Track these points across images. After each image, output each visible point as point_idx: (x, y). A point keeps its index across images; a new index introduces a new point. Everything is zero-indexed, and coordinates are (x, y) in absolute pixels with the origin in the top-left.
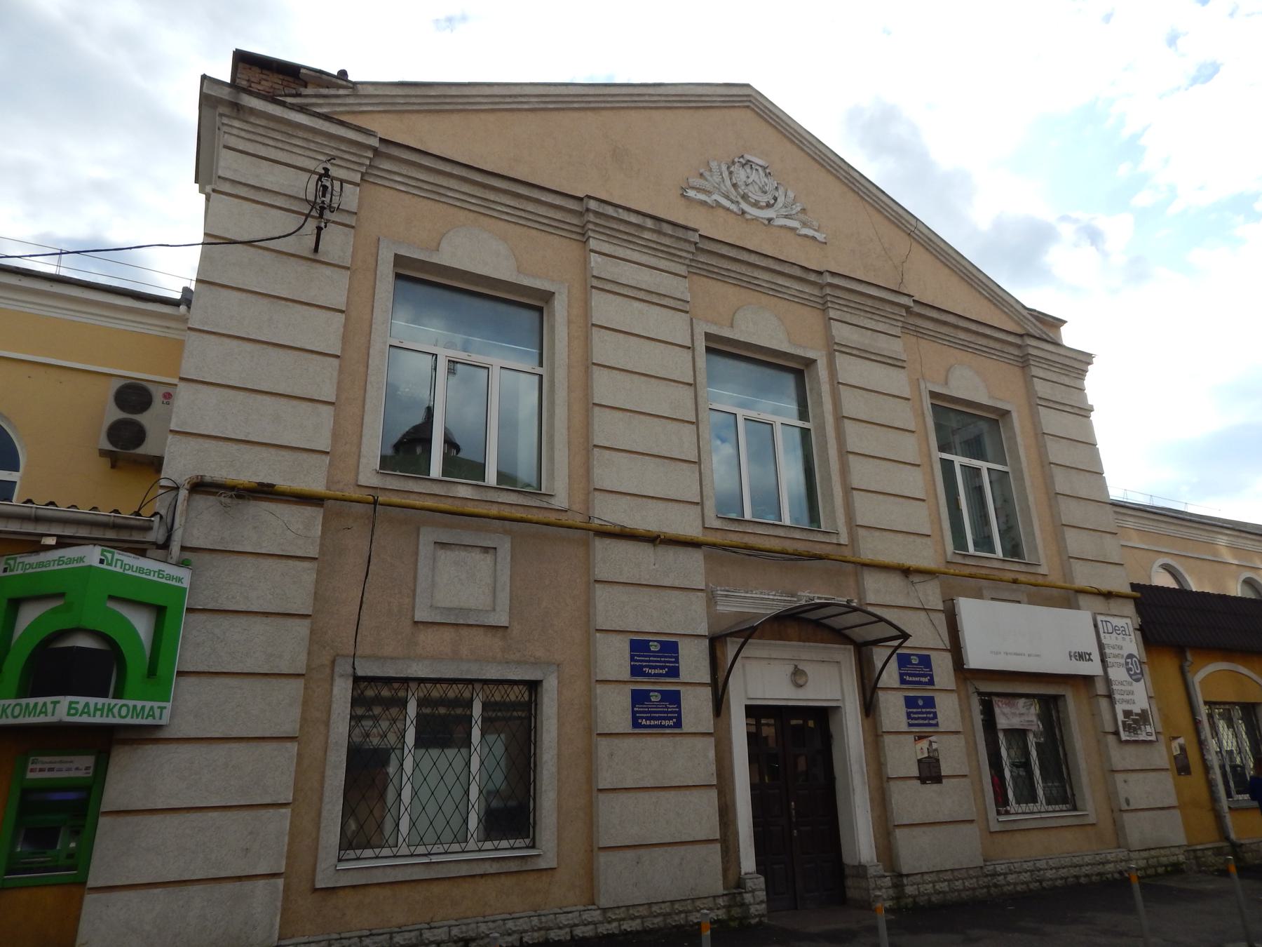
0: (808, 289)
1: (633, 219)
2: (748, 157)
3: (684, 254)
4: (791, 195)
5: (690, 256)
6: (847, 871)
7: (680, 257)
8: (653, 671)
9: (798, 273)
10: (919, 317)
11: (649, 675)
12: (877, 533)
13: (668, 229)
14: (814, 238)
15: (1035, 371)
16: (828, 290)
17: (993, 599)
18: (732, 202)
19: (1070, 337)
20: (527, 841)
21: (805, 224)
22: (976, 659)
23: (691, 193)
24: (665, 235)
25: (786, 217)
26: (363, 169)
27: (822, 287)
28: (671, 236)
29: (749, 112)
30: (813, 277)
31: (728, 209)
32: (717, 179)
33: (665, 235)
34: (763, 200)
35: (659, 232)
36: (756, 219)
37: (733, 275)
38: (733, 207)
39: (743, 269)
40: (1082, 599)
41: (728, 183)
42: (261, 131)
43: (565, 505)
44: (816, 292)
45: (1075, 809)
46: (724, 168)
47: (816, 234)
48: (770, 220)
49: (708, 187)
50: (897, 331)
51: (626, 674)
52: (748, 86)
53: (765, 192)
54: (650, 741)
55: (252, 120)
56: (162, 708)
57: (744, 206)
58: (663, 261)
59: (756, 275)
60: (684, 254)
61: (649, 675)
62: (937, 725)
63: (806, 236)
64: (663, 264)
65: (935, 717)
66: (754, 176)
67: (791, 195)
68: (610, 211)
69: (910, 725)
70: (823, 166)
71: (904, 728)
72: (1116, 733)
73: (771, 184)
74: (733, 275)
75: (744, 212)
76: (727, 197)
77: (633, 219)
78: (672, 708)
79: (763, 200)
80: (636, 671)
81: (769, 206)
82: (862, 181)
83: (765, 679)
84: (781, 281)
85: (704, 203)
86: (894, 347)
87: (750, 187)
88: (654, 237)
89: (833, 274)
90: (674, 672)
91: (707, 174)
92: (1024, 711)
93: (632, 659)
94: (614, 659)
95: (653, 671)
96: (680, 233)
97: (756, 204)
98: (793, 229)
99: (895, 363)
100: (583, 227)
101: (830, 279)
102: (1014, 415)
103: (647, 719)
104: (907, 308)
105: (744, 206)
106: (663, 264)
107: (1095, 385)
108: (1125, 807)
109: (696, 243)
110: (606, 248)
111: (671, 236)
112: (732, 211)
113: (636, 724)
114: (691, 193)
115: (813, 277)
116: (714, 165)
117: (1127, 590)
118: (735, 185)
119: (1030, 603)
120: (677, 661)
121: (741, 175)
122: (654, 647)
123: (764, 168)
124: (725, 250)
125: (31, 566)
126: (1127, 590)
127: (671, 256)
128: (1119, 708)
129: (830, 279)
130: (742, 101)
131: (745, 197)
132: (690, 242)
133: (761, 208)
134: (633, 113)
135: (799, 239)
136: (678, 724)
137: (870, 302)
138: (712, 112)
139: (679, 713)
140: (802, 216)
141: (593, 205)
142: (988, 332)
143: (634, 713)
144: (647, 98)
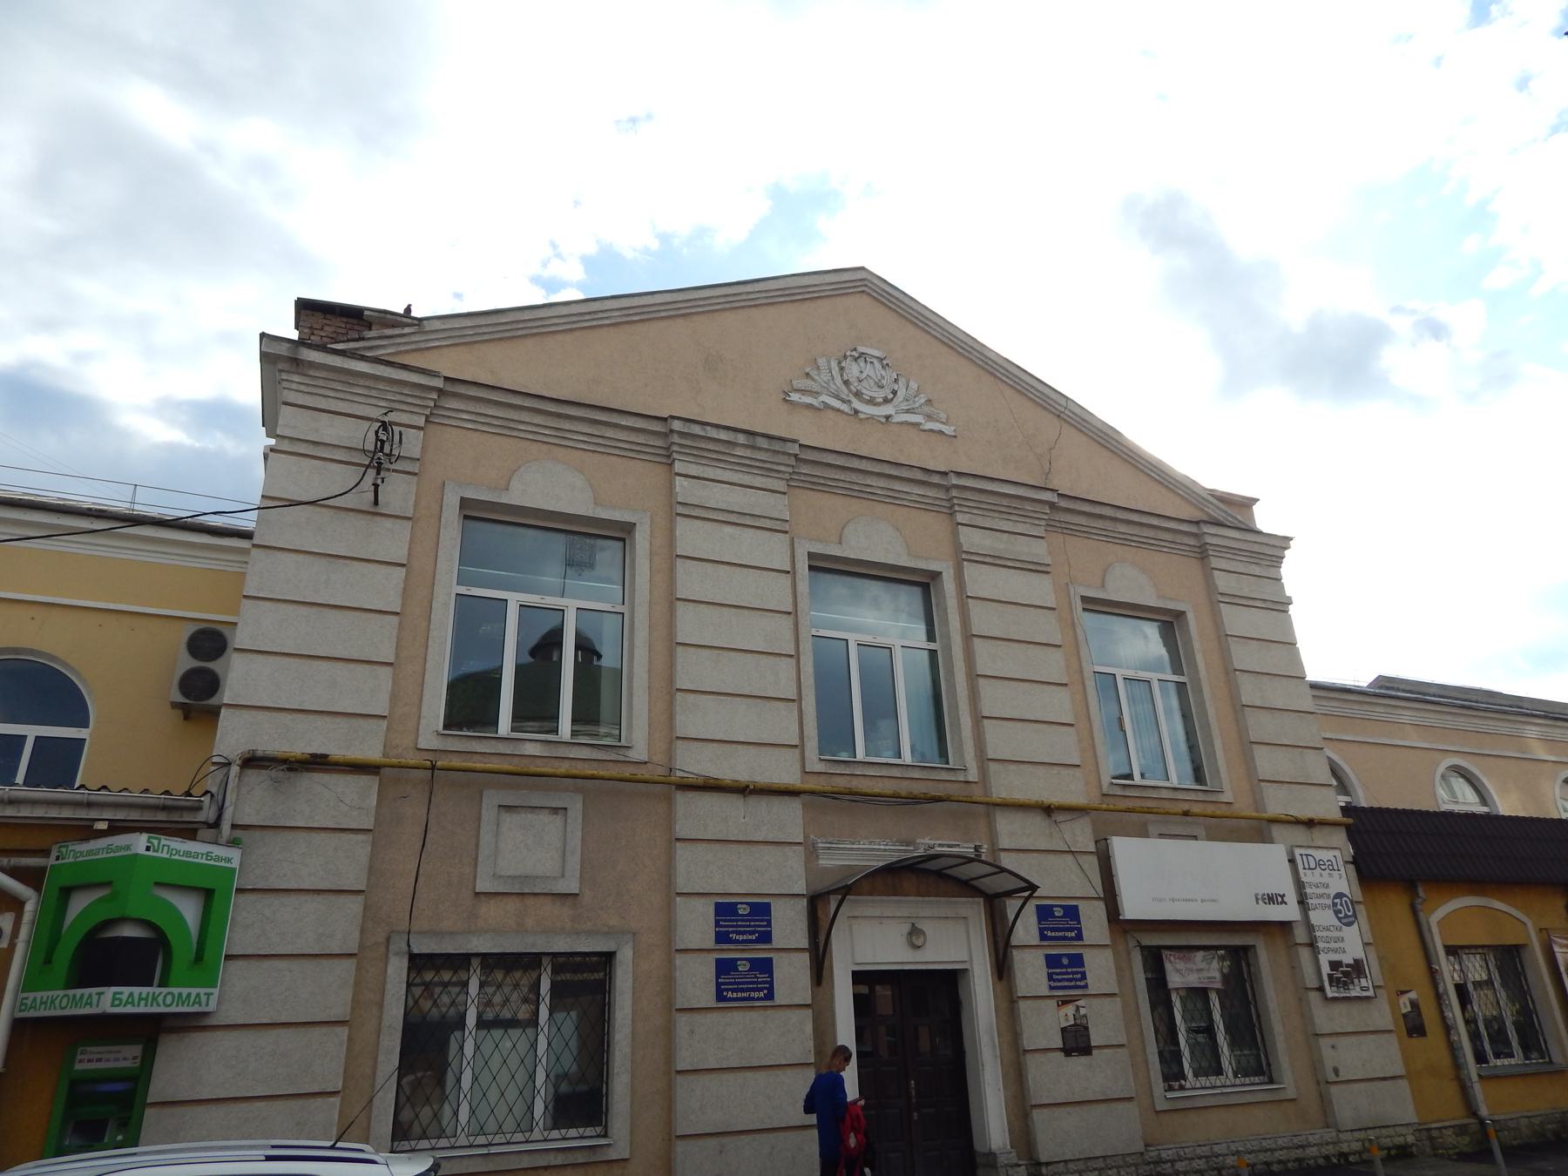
0: (931, 493)
1: (723, 435)
2: (861, 349)
3: (782, 468)
4: (914, 385)
6: (978, 1160)
8: (741, 938)
9: (919, 476)
10: (1066, 513)
11: (737, 942)
12: (1013, 767)
14: (941, 432)
15: (1215, 563)
16: (954, 493)
17: (1162, 836)
18: (844, 401)
19: (1266, 520)
20: (599, 1129)
21: (929, 417)
22: (1134, 907)
23: (795, 397)
24: (760, 449)
25: (908, 411)
27: (948, 489)
28: (767, 450)
30: (936, 479)
32: (825, 377)
33: (760, 449)
35: (753, 447)
36: (872, 418)
38: (844, 407)
39: (854, 477)
40: (1276, 830)
41: (838, 381)
42: (321, 383)
43: (644, 757)
45: (1271, 1081)
46: (834, 364)
48: (887, 417)
49: (816, 388)
50: (1040, 532)
51: (710, 942)
52: (862, 269)
54: (737, 1016)
55: (311, 373)
56: (208, 995)
57: (857, 405)
59: (868, 482)
60: (782, 468)
61: (737, 942)
62: (1086, 986)
63: (932, 431)
64: (758, 481)
65: (1084, 977)
66: (868, 370)
67: (914, 385)
68: (697, 430)
69: (1051, 988)
71: (1047, 993)
72: (1321, 989)
73: (889, 375)
75: (856, 412)
76: (837, 397)
77: (723, 435)
78: (763, 977)
79: (880, 395)
80: (721, 938)
81: (886, 401)
83: (875, 940)
84: (897, 486)
85: (810, 406)
86: (1037, 550)
87: (865, 383)
88: (748, 453)
89: (959, 474)
90: (766, 937)
91: (813, 373)
92: (1203, 965)
93: (717, 924)
94: (697, 925)
95: (741, 938)
96: (777, 446)
97: (871, 402)
98: (916, 425)
99: (1039, 569)
100: (666, 435)
101: (955, 481)
102: (1190, 616)
103: (733, 991)
104: (1052, 505)
105: (857, 405)
106: (758, 481)
107: (1293, 574)
108: (1332, 1077)
110: (694, 470)
111: (767, 450)
113: (720, 997)
114: (795, 397)
115: (936, 479)
116: (822, 362)
117: (1336, 815)
118: (846, 383)
119: (1211, 838)
120: (769, 925)
121: (853, 370)
122: (743, 910)
123: (881, 360)
125: (178, 852)
126: (1336, 815)
128: (1324, 960)
129: (955, 481)
130: (858, 287)
131: (858, 394)
133: (878, 404)
134: (727, 314)
136: (770, 995)
137: (1005, 502)
138: (820, 302)
139: (771, 983)
140: (927, 409)
141: (677, 425)
142: (1136, 518)
143: (718, 985)
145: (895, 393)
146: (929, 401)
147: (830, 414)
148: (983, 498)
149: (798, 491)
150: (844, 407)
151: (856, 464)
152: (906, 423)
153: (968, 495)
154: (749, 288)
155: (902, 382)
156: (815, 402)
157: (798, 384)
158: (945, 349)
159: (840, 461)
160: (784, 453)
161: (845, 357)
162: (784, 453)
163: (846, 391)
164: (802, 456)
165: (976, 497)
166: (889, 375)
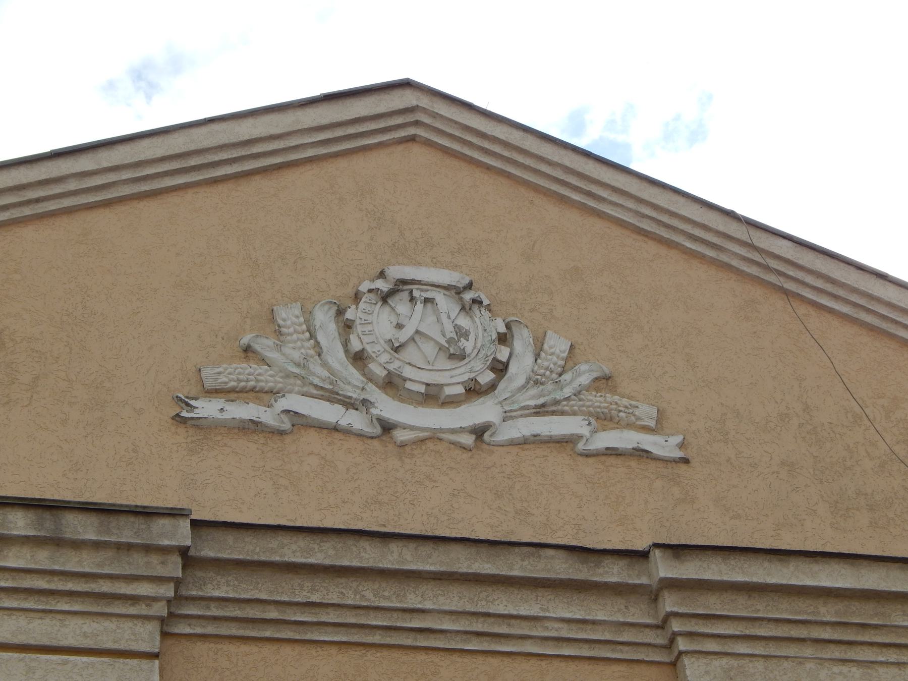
2: (397, 272)
3: (144, 589)
4: (557, 345)
5: (168, 591)
7: (134, 599)
9: (561, 567)
13: (84, 528)
14: (641, 454)
16: (670, 603)
18: (349, 404)
21: (605, 420)
23: (207, 408)
24: (77, 545)
25: (541, 410)
26: (160, 609)
27: (653, 594)
28: (97, 545)
29: (416, 150)
30: (613, 573)
31: (335, 429)
32: (297, 349)
33: (77, 545)
34: (453, 378)
35: (57, 542)
36: (434, 436)
37: (331, 617)
38: (355, 420)
39: (369, 593)
41: (337, 357)
44: (638, 613)
46: (324, 318)
47: (648, 442)
48: (479, 432)
49: (266, 377)
52: (406, 84)
53: (461, 356)
57: (388, 408)
58: (75, 624)
59: (412, 600)
60: (144, 589)
63: (612, 452)
64: (72, 632)
66: (416, 318)
67: (557, 345)
70: (563, 200)
73: (481, 329)
74: (331, 617)
75: (387, 427)
76: (332, 396)
79: (453, 378)
81: (474, 391)
82: (530, 144)
84: (502, 603)
85: (252, 427)
87: (410, 353)
88: (42, 558)
89: (678, 550)
91: (265, 345)
96: (127, 531)
97: (432, 396)
98: (566, 442)
100: (662, 626)
101: (664, 568)
105: (388, 408)
106: (72, 632)
109: (184, 552)
111: (97, 545)
112: (347, 432)
114: (207, 408)
115: (613, 573)
116: (289, 315)
118: (359, 358)
121: (377, 325)
123: (456, 291)
124: (293, 551)
127: (101, 601)
129: (664, 568)
130: (396, 124)
131: (392, 384)
132: (165, 550)
133: (452, 402)
134: (28, 233)
135: (589, 467)
137: (827, 611)
138: (289, 176)
140: (598, 400)
144: (72, 185)
145: (500, 368)
146: (605, 381)
147: (311, 440)
148: (761, 607)
149: (201, 648)
150: (355, 420)
151: (368, 555)
152: (535, 441)
153: (714, 604)
154: (85, 163)
155: (522, 342)
156: (266, 416)
157: (212, 376)
158: (652, 248)
159: (323, 553)
160: (148, 549)
161: (357, 297)
162: (148, 549)
163: (353, 374)
164: (208, 552)
165: (741, 606)
166: (481, 329)
